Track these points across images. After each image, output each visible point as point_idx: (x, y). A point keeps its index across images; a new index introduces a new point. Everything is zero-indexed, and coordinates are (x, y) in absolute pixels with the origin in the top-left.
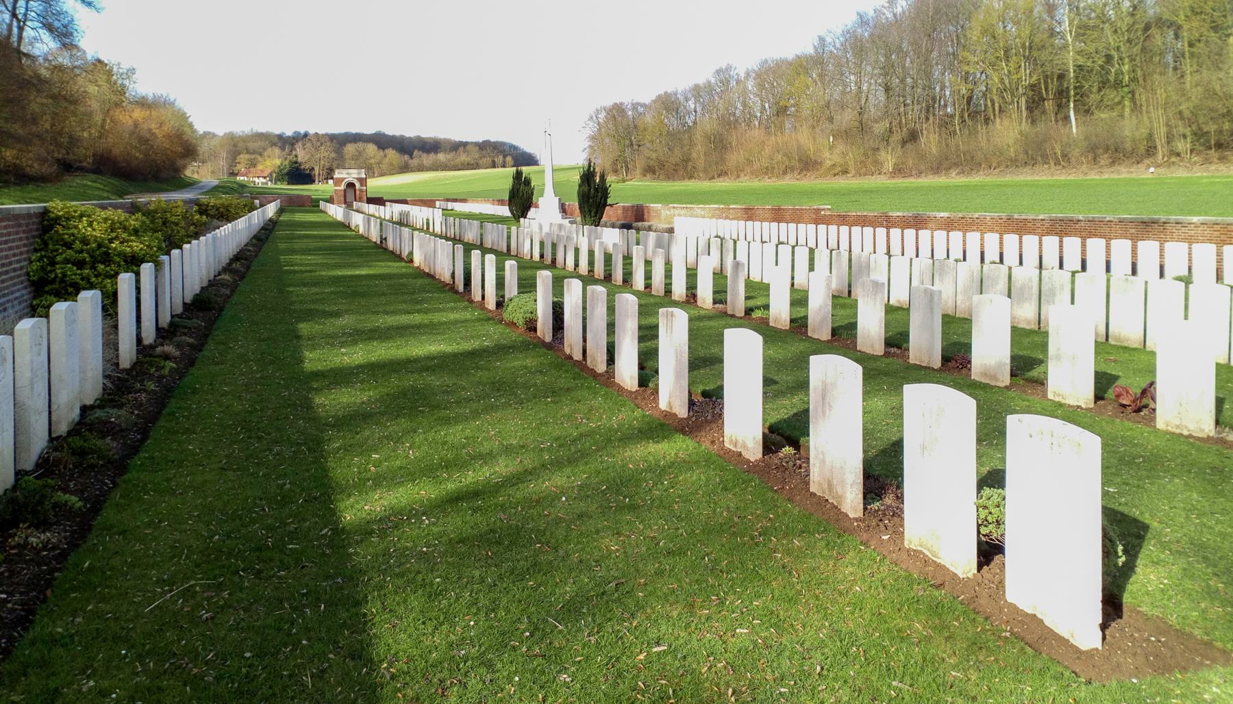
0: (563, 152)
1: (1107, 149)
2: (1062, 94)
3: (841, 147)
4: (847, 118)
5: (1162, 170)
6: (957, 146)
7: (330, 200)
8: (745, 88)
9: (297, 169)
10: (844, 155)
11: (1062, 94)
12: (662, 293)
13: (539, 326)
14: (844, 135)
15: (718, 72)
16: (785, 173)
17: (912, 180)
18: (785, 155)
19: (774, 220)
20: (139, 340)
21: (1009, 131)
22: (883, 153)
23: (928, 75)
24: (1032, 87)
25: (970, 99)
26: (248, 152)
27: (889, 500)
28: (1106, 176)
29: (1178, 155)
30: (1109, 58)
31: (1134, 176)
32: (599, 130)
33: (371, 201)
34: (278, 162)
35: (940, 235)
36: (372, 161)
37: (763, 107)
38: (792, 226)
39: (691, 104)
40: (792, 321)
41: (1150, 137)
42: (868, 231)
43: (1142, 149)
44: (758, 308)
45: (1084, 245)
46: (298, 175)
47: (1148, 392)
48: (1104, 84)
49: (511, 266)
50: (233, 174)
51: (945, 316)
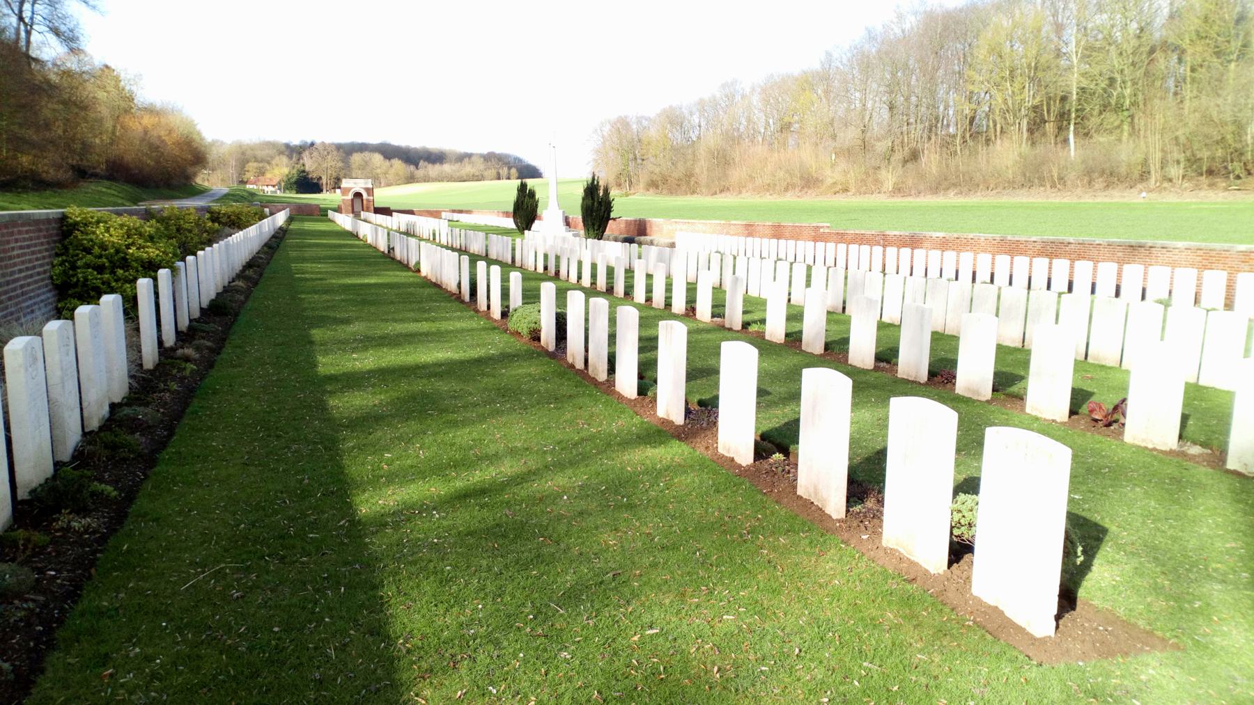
1: (1103, 173)
2: (1063, 116)
3: (843, 165)
4: (850, 136)
5: (1154, 195)
6: (957, 167)
7: (338, 210)
9: (305, 178)
10: (845, 172)
11: (1063, 116)
12: (662, 305)
14: (847, 153)
15: (724, 86)
16: (786, 189)
17: (910, 199)
18: (787, 171)
20: (160, 342)
21: (1009, 151)
23: (933, 93)
24: (1035, 108)
26: (256, 161)
27: (870, 503)
30: (1112, 81)
31: (1125, 200)
33: (378, 211)
34: (286, 171)
36: (379, 171)
37: (768, 123)
40: (787, 335)
43: (1136, 174)
44: (755, 322)
46: (307, 184)
48: (1105, 107)
50: (243, 182)
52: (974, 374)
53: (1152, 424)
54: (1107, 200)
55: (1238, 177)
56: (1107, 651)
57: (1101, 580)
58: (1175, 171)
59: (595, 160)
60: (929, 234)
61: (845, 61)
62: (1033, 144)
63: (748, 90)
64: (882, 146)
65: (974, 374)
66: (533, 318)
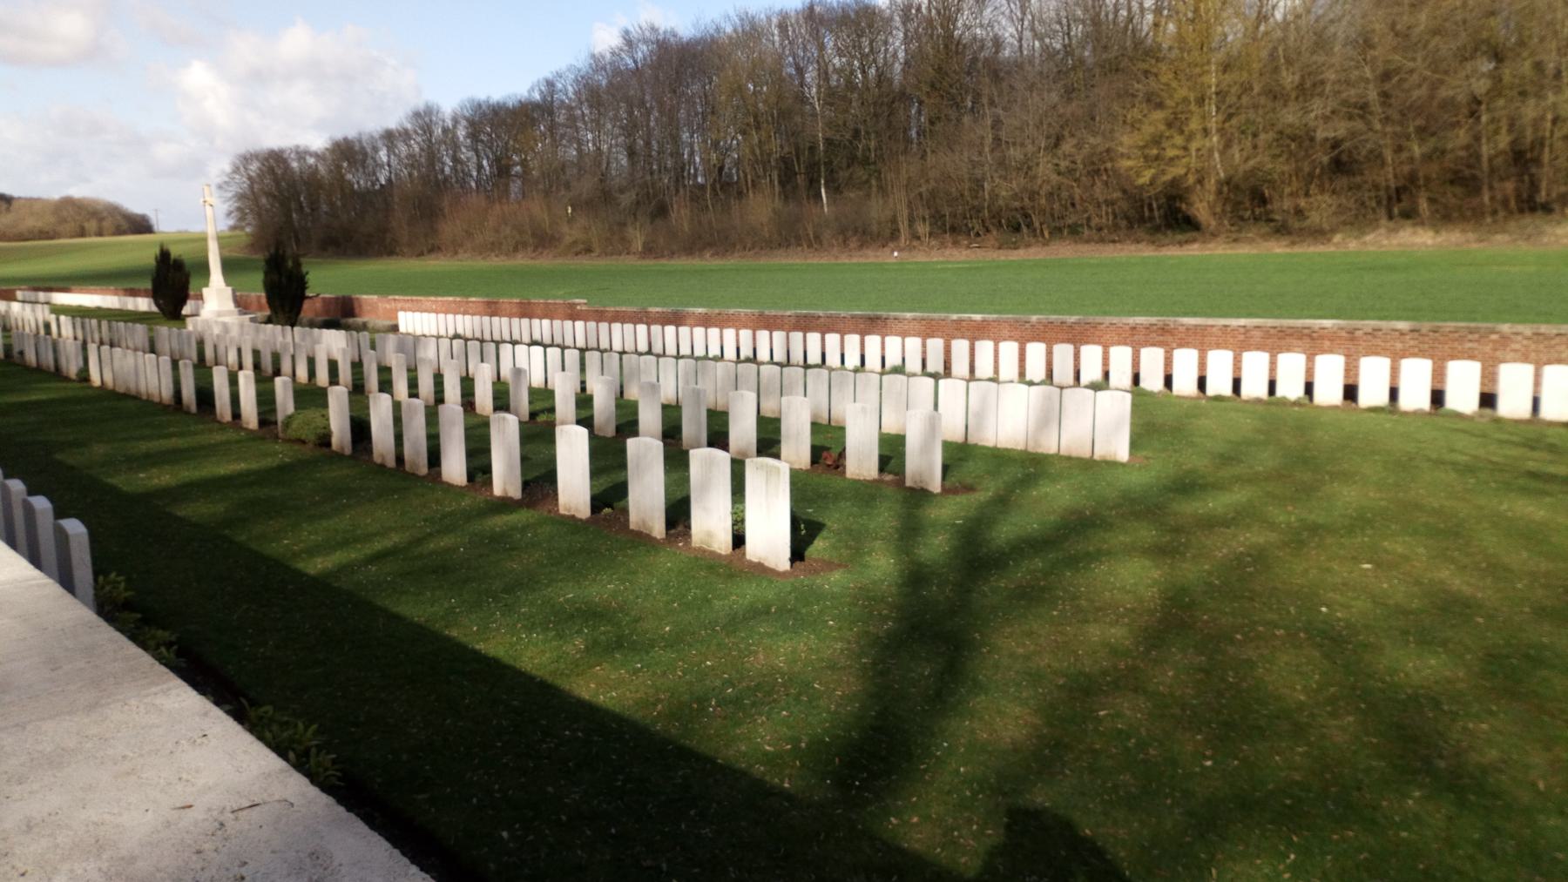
0: (197, 208)
1: (856, 231)
2: (813, 167)
3: (582, 221)
4: (586, 186)
5: (905, 254)
6: (710, 223)
8: (455, 136)
10: (586, 229)
11: (813, 167)
12: (1425, 403)
13: (335, 440)
14: (585, 205)
16: (516, 249)
17: (664, 261)
19: (522, 316)
21: (761, 208)
22: (630, 230)
23: (675, 139)
24: (783, 159)
25: (721, 169)
27: (680, 528)
28: (855, 260)
29: (918, 238)
30: (856, 133)
31: (880, 260)
32: (251, 187)
35: (699, 331)
37: (480, 167)
38: (546, 322)
39: (383, 155)
41: (894, 220)
42: (629, 327)
43: (887, 232)
44: (542, 411)
45: (823, 340)
47: (842, 455)
48: (852, 160)
49: (285, 383)
51: (709, 411)
52: (743, 430)
53: (861, 461)
54: (862, 260)
55: (978, 235)
56: (816, 572)
57: (819, 547)
58: (922, 229)
59: (239, 209)
60: (691, 310)
61: (571, 94)
62: (786, 198)
63: (450, 124)
64: (626, 199)
65: (743, 430)
66: (319, 422)
